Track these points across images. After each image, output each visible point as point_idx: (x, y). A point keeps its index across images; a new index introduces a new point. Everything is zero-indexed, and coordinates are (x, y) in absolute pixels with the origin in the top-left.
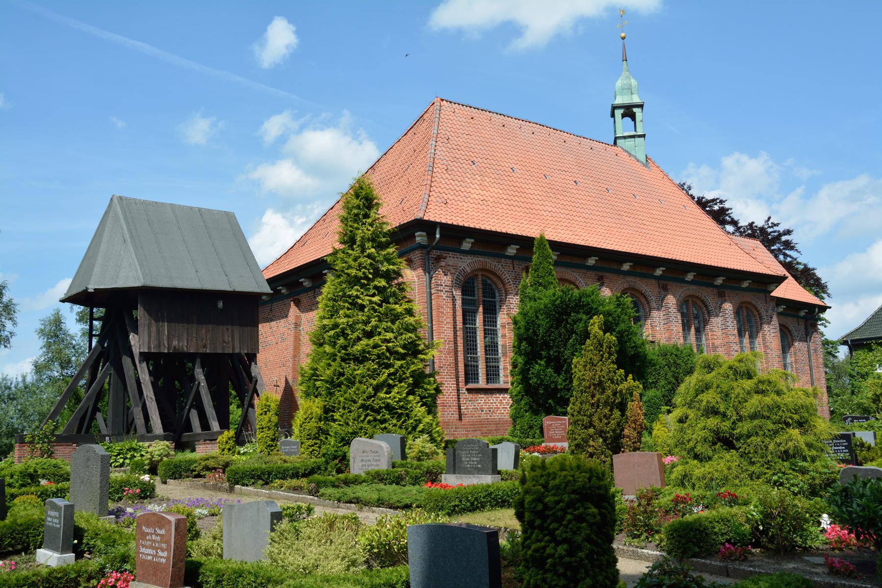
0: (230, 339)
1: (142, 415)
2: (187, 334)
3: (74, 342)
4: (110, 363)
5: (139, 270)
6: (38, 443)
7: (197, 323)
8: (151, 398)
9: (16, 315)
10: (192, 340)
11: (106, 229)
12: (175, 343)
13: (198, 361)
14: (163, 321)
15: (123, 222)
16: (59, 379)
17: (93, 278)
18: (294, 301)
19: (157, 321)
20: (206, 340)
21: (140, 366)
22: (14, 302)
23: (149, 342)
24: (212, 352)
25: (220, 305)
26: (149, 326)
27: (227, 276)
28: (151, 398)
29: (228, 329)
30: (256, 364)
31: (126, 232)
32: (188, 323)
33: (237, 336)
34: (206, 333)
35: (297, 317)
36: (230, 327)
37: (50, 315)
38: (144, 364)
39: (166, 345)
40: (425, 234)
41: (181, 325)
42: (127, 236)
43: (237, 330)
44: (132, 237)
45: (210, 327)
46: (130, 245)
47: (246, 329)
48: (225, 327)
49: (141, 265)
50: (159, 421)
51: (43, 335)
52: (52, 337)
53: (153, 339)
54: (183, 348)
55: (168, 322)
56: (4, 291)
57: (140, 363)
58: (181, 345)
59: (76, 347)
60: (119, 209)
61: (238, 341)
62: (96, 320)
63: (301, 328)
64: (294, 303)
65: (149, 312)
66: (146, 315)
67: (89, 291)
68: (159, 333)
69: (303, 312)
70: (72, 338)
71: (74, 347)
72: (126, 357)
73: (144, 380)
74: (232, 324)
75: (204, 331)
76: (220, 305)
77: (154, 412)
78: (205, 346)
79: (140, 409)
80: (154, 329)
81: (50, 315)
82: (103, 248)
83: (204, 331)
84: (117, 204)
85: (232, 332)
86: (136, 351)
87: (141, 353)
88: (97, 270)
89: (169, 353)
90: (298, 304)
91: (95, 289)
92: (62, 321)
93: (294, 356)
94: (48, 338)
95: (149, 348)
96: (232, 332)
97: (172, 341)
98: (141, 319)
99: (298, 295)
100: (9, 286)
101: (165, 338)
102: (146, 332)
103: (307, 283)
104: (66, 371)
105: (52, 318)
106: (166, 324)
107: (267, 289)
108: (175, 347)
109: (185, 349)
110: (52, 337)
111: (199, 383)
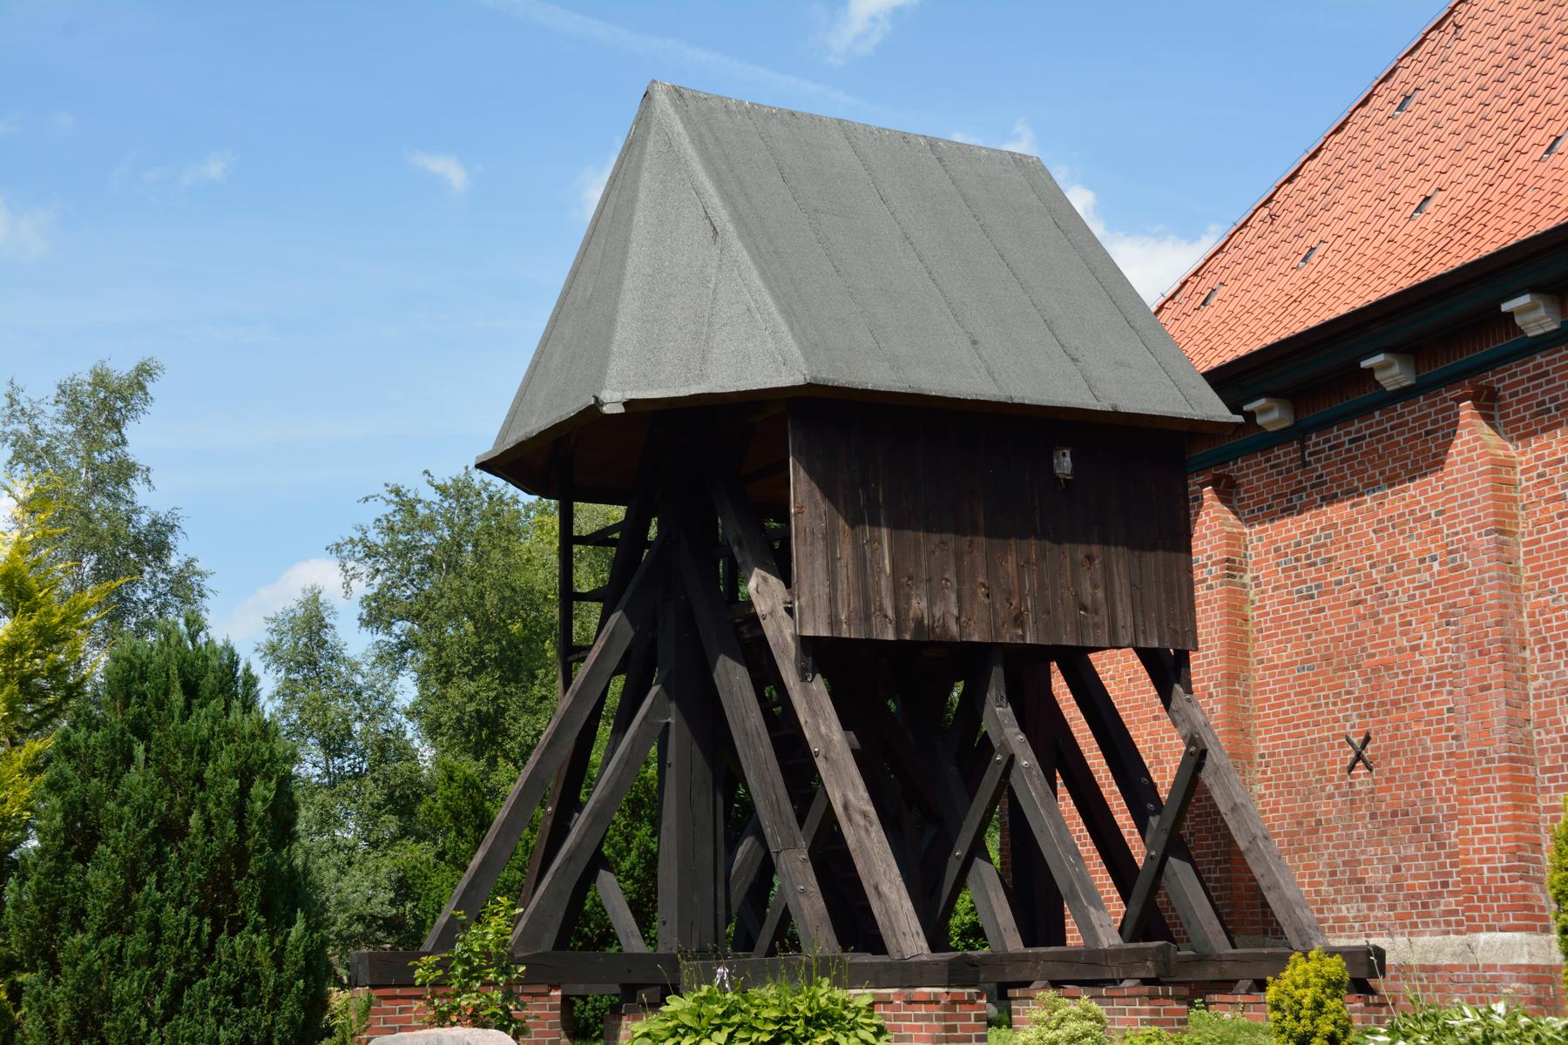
0: (1100, 594)
1: (813, 880)
2: (958, 575)
3: (359, 680)
4: (666, 687)
5: (784, 328)
6: (465, 988)
7: (988, 535)
8: (865, 815)
9: (205, 602)
10: (974, 593)
11: (642, 195)
12: (919, 605)
13: (997, 676)
14: (875, 523)
15: (697, 166)
16: (321, 786)
17: (616, 366)
18: (1215, 483)
19: (855, 521)
20: (1022, 598)
21: (806, 693)
22: (199, 566)
23: (832, 600)
24: (1043, 641)
25: (1064, 464)
26: (830, 539)
27: (1074, 360)
28: (865, 815)
29: (1090, 558)
30: (1189, 691)
31: (715, 201)
32: (958, 530)
33: (1121, 586)
34: (1020, 568)
35: (1500, 467)
36: (1095, 549)
37: (294, 605)
38: (819, 685)
39: (890, 613)
41: (935, 538)
42: (722, 216)
43: (1120, 558)
44: (739, 219)
45: (1032, 547)
46: (737, 246)
47: (1151, 558)
48: (1081, 551)
49: (788, 313)
50: (908, 905)
51: (278, 659)
52: (299, 665)
53: (843, 587)
54: (945, 626)
55: (896, 524)
56: (171, 539)
57: (804, 679)
58: (938, 613)
59: (365, 695)
60: (679, 127)
61: (1127, 600)
62: (583, 540)
63: (1247, 578)
64: (1217, 492)
65: (827, 485)
66: (818, 495)
67: (606, 410)
68: (862, 564)
69: (1249, 522)
70: (354, 668)
71: (358, 694)
72: (731, 663)
73: (828, 743)
74: (1105, 541)
75: (1011, 565)
76: (1064, 464)
77: (880, 867)
78: (1018, 621)
79: (805, 855)
80: (845, 551)
81: (294, 605)
82: (638, 259)
83: (1011, 565)
84: (671, 111)
85: (1107, 569)
86: (781, 634)
87: (809, 646)
88: (626, 333)
89: (899, 644)
90: (1489, 406)
91: (628, 404)
92: (327, 620)
93: (1231, 677)
94: (289, 670)
95: (833, 622)
96: (1107, 569)
97: (908, 599)
98: (800, 512)
99: (1225, 463)
100: (184, 524)
101: (885, 584)
102: (820, 563)
103: (1275, 415)
104: (337, 761)
105: (300, 612)
106: (885, 532)
107: (1213, 408)
108: (919, 622)
109: (954, 628)
110: (299, 665)
111: (1011, 759)
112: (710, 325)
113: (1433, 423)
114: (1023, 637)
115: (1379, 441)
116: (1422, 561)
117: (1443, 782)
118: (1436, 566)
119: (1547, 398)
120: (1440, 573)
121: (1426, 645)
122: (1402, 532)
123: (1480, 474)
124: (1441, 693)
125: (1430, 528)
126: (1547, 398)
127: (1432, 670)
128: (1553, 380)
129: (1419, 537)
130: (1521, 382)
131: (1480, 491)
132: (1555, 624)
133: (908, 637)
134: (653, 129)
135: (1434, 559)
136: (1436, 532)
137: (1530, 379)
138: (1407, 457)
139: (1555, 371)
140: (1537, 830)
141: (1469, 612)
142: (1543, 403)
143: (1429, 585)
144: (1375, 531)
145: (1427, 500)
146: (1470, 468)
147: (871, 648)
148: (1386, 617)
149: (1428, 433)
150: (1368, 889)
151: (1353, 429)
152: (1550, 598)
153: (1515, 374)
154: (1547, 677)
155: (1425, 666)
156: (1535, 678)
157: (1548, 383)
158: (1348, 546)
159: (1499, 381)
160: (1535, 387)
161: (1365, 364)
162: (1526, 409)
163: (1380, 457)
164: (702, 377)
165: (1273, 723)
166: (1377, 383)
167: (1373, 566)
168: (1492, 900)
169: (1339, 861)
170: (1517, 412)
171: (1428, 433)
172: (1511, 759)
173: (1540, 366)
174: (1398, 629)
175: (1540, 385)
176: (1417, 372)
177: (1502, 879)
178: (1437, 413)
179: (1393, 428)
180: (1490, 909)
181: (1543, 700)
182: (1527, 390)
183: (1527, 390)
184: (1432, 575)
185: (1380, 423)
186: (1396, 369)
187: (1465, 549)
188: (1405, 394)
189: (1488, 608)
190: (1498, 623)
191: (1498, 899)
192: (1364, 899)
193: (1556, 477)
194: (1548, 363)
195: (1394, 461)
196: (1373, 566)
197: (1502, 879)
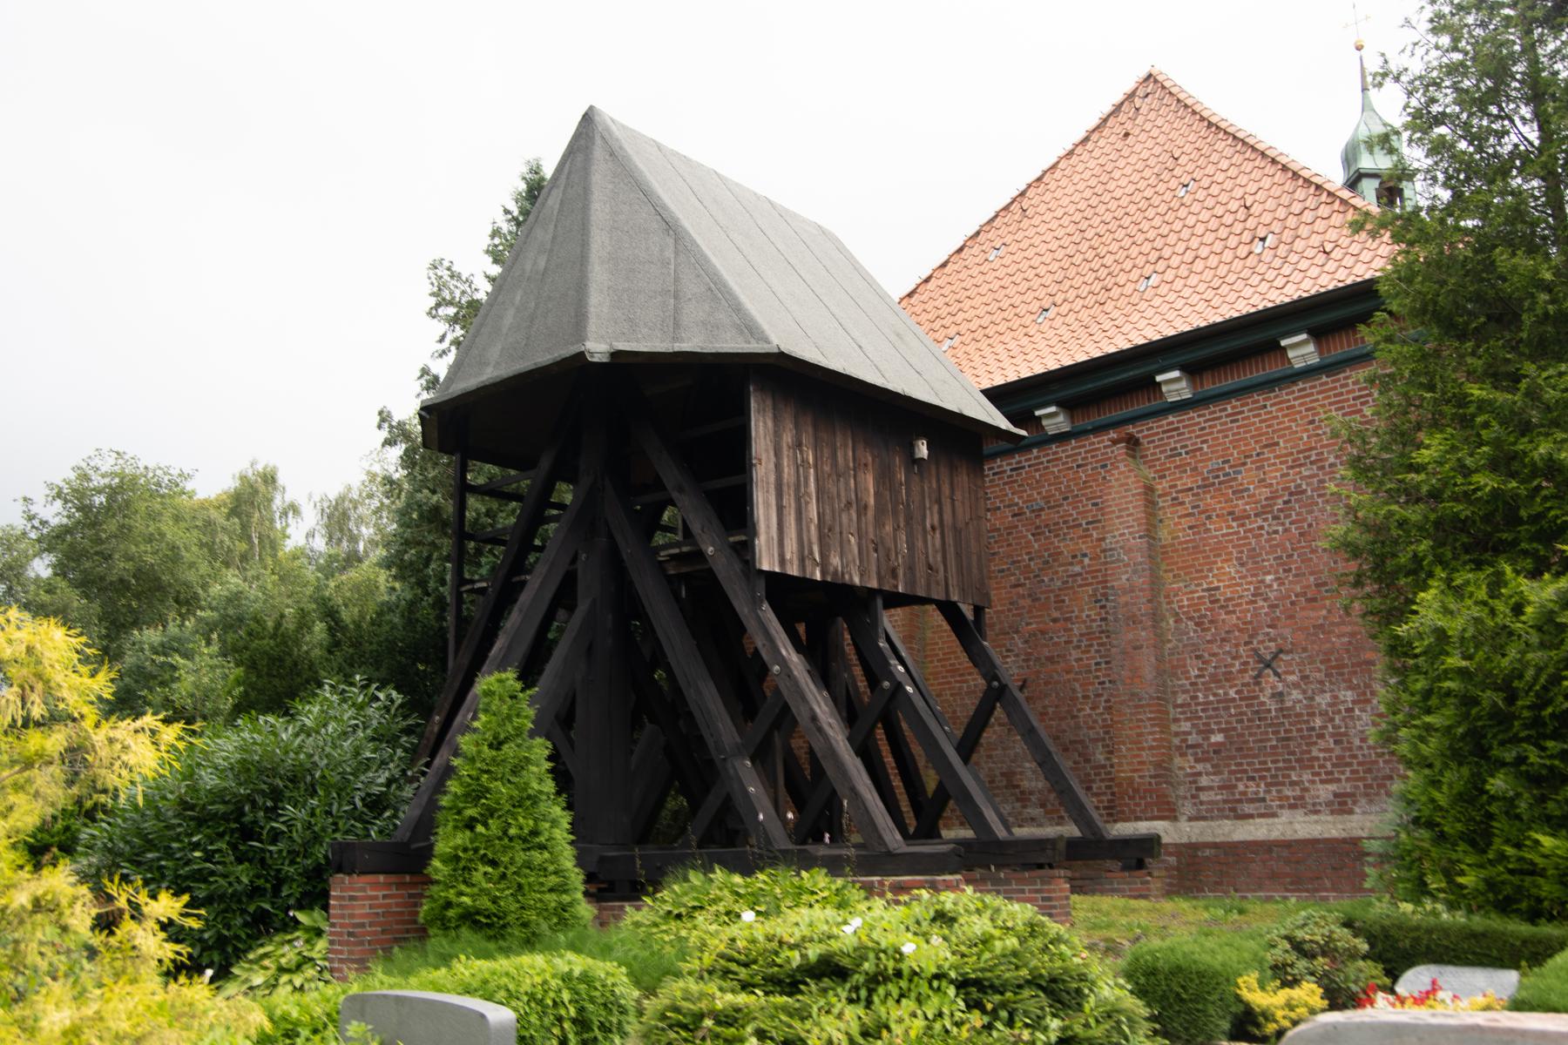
0: (939, 558)
25: (923, 450)
40: (1304, 336)
89: (823, 583)
91: (616, 354)
95: (782, 561)
101: (813, 528)
112: (676, 297)
113: (1083, 459)
114: (896, 587)
115: (1037, 470)
116: (1074, 557)
117: (1090, 715)
118: (1086, 561)
119: (1178, 445)
120: (1089, 566)
121: (1077, 617)
122: (1056, 536)
123: (1133, 495)
124: (1089, 652)
125: (1081, 533)
126: (1178, 445)
127: (1081, 635)
128: (1183, 434)
129: (1072, 539)
130: (1158, 434)
131: (1134, 507)
132: (1186, 603)
133: (829, 579)
134: (598, 141)
135: (1085, 555)
136: (1086, 536)
137: (1164, 432)
138: (1061, 483)
139: (1184, 427)
140: (1170, 748)
141: (1125, 593)
142: (1176, 449)
143: (1080, 574)
144: (1033, 535)
145: (1078, 513)
146: (1126, 491)
147: (804, 583)
148: (1043, 596)
149: (1078, 466)
150: (1022, 793)
151: (1014, 461)
152: (1181, 585)
153: (1152, 428)
154: (1180, 641)
155: (1076, 632)
156: (1170, 641)
157: (1179, 435)
158: (1009, 545)
159: (1138, 432)
160: (1168, 438)
161: (1037, 413)
162: (1161, 452)
163: (1037, 482)
164: (675, 339)
165: (941, 672)
166: (1043, 427)
167: (1030, 560)
168: (1140, 798)
169: (997, 772)
170: (1153, 454)
171: (1078, 466)
172: (1158, 698)
173: (1172, 423)
174: (1053, 605)
175: (1173, 437)
176: (1073, 422)
177: (1150, 783)
178: (1086, 452)
179: (1048, 462)
180: (1138, 805)
181: (1176, 656)
182: (1162, 439)
183: (1162, 439)
184: (1083, 568)
185: (1036, 458)
186: (1061, 418)
187: (1121, 548)
188: (1062, 438)
189: (1141, 590)
190: (1149, 601)
191: (1145, 798)
192: (1018, 800)
193: (1187, 500)
194: (1178, 422)
195: (1049, 485)
196: (1030, 560)
197: (1150, 783)
